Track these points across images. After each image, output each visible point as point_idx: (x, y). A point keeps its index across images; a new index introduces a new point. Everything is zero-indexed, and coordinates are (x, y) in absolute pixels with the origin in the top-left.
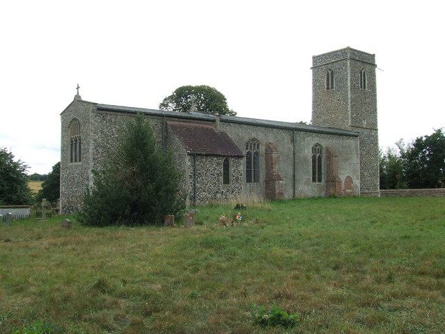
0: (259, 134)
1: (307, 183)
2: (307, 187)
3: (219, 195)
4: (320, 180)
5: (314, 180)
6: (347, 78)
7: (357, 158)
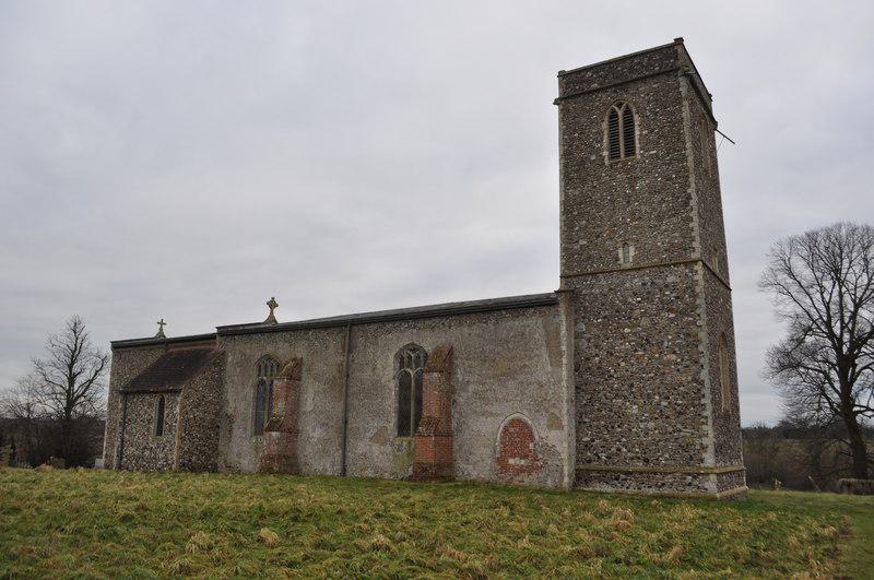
0: (282, 349)
1: (380, 437)
3: (147, 453)
5: (403, 429)
6: (636, 123)
7: (555, 355)
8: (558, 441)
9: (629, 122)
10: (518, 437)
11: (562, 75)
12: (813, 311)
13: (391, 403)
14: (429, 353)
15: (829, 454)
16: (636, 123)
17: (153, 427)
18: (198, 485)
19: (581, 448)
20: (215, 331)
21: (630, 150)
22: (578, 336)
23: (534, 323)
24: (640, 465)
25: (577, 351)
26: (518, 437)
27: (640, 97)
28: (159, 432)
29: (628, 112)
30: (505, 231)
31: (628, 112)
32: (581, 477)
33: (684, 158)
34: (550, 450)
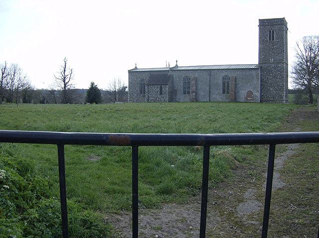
2: (217, 95)
4: (228, 93)
5: (224, 92)
6: (273, 32)
8: (257, 94)
9: (273, 33)
10: (250, 94)
11: (130, 72)
12: (299, 52)
13: (221, 87)
14: (244, 72)
15: (306, 95)
16: (273, 32)
17: (159, 93)
18: (174, 104)
19: (261, 96)
20: (125, 82)
21: (273, 39)
22: (261, 75)
23: (254, 72)
24: (272, 99)
25: (261, 78)
26: (250, 94)
27: (276, 28)
28: (161, 94)
29: (273, 31)
30: (247, 54)
31: (273, 31)
32: (261, 101)
33: (283, 43)
34: (256, 96)
